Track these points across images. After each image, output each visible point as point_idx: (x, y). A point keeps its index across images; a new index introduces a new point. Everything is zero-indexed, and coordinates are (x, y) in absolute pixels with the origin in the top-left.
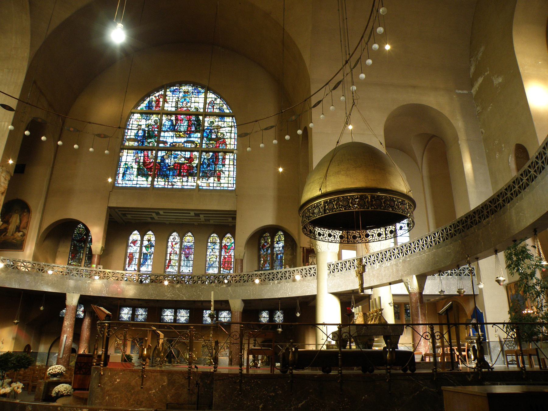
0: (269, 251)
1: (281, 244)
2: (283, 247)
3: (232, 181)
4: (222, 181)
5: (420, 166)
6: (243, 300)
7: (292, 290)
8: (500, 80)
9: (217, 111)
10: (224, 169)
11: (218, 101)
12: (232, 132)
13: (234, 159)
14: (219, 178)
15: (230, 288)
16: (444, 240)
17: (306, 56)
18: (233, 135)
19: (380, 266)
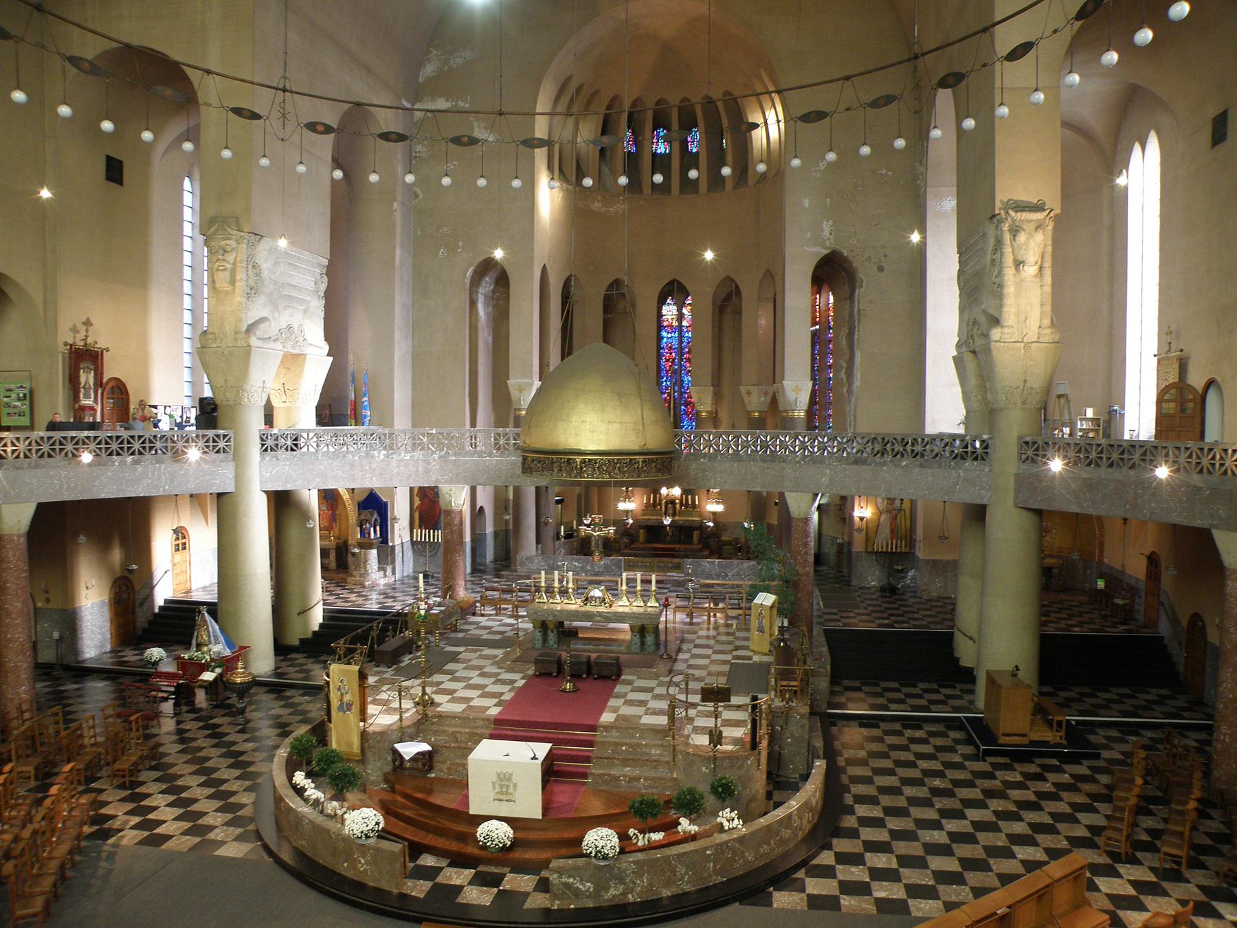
7: (172, 481)
19: (387, 456)
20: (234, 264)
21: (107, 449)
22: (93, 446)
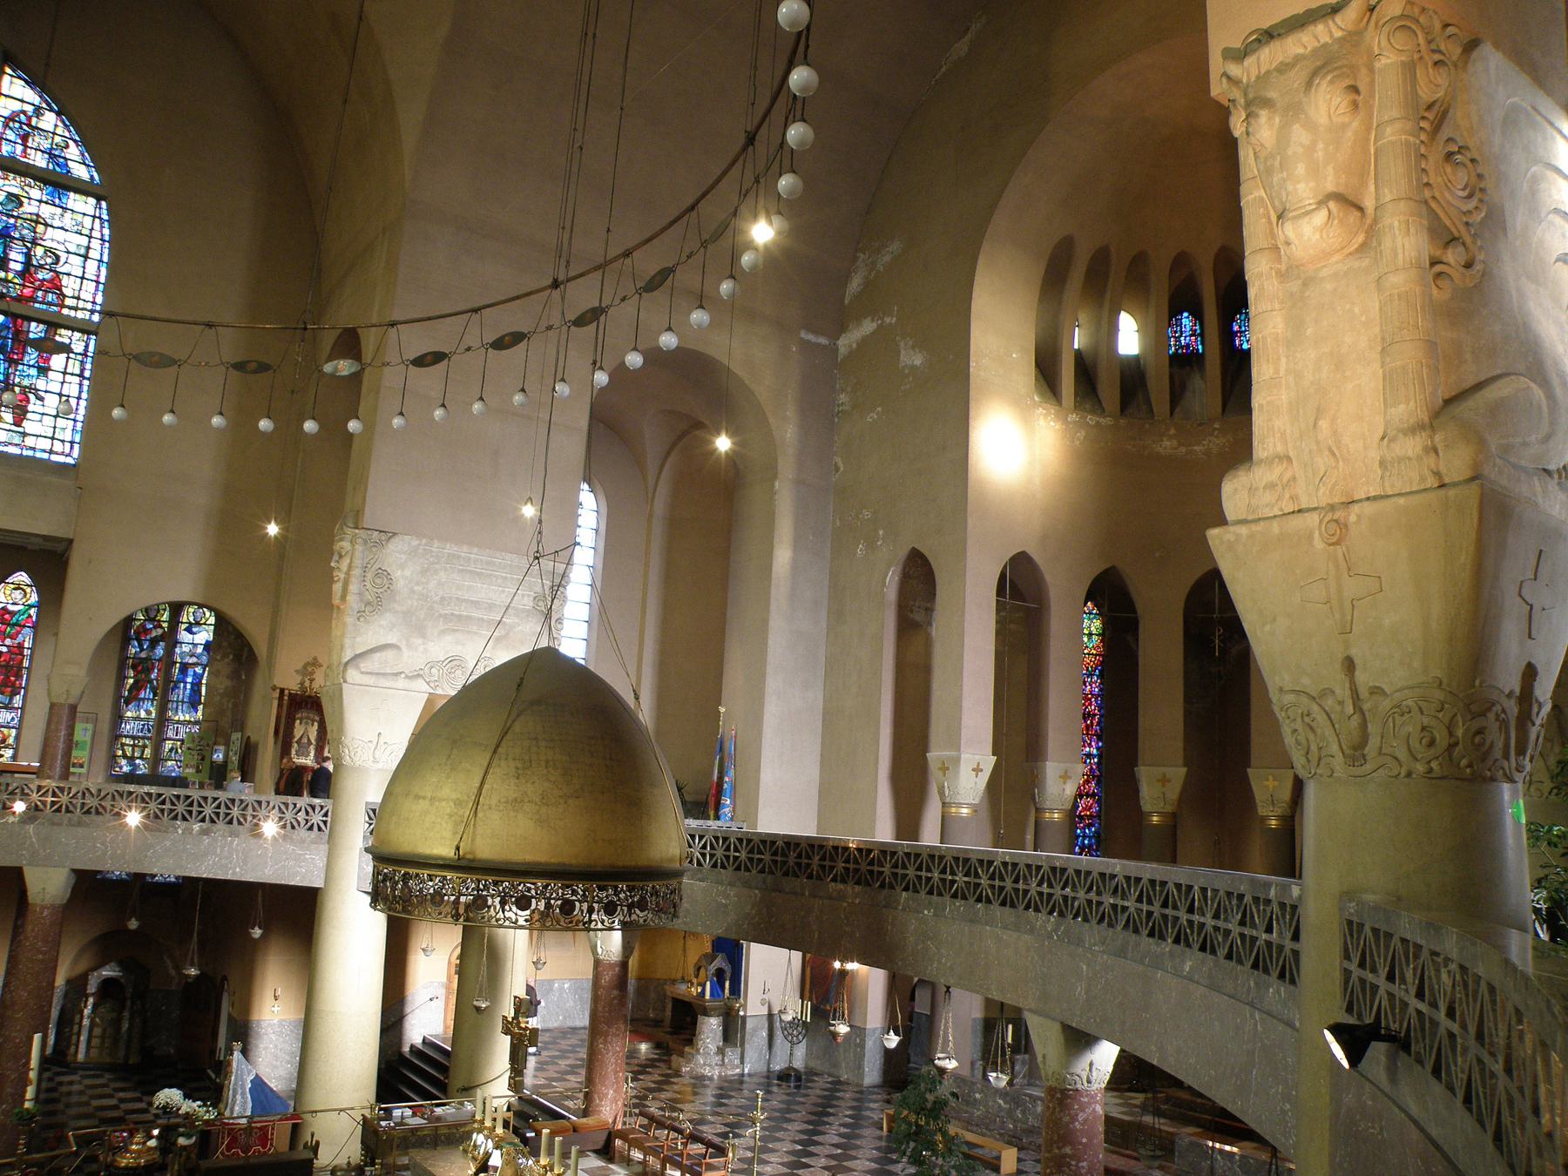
0: (160, 651)
1: (204, 636)
2: (208, 646)
3: (66, 430)
4: (28, 426)
5: (650, 489)
6: (74, 871)
7: (245, 862)
8: (918, 360)
9: (40, 161)
10: (41, 384)
11: (49, 120)
12: (92, 254)
13: (85, 355)
14: (20, 414)
15: (31, 828)
16: (715, 866)
17: (410, 119)
18: (92, 266)
20: (348, 573)
21: (172, 811)
22: (153, 806)
